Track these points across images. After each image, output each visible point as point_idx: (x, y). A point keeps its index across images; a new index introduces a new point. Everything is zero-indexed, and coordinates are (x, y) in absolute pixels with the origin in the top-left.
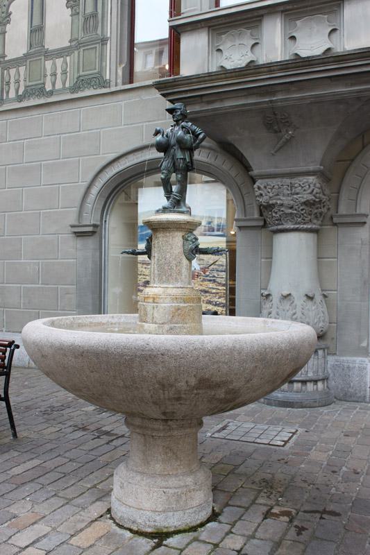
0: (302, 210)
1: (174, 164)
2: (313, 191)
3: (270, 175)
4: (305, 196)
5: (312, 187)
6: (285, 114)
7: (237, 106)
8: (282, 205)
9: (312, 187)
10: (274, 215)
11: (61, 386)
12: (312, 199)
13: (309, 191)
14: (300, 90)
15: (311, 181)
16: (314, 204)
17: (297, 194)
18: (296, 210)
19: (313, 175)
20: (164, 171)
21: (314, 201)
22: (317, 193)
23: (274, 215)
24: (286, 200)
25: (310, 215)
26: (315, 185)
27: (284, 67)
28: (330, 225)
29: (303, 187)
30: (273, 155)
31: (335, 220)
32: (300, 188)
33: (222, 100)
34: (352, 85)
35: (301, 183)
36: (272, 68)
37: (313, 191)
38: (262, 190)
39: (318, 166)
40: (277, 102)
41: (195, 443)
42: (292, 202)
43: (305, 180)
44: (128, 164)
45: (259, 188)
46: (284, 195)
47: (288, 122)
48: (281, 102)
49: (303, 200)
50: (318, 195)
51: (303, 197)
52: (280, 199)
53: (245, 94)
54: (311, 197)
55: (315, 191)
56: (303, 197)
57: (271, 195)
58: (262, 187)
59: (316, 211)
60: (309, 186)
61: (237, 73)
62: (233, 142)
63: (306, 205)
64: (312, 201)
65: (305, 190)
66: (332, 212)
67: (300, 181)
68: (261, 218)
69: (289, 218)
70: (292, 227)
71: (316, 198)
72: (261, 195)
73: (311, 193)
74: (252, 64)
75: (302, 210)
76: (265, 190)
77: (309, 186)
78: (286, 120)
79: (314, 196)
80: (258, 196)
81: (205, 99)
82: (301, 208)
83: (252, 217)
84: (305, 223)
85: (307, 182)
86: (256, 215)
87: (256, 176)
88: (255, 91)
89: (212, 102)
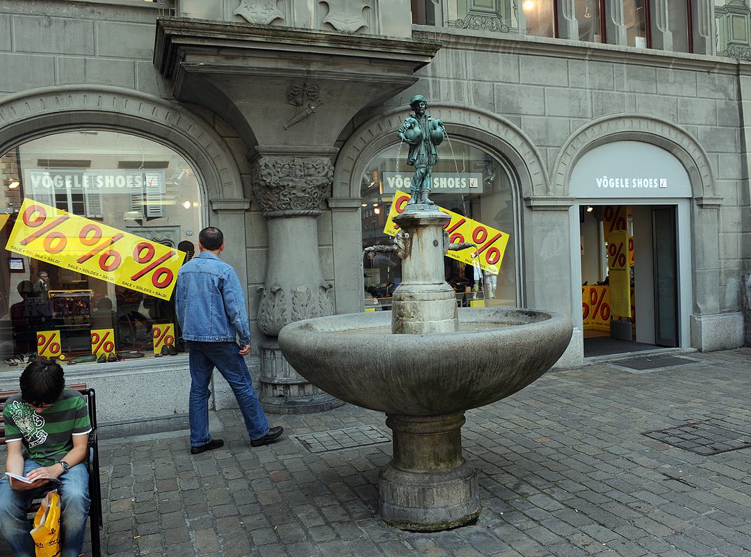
5: (326, 171)
6: (316, 87)
7: (267, 69)
8: (294, 187)
10: (282, 197)
11: (106, 439)
15: (325, 162)
17: (310, 176)
18: (308, 193)
19: (327, 156)
23: (282, 197)
24: (301, 183)
29: (316, 169)
30: (286, 129)
31: (332, 205)
33: (245, 58)
34: (389, 71)
35: (315, 164)
40: (314, 73)
41: (454, 438)
42: (305, 185)
44: (29, 114)
45: (266, 165)
46: (296, 176)
47: (313, 96)
48: (319, 74)
52: (292, 180)
53: (275, 56)
57: (281, 175)
58: (271, 166)
62: (239, 108)
69: (300, 202)
70: (302, 212)
73: (326, 175)
74: (276, 24)
78: (314, 94)
80: (265, 176)
81: (222, 53)
82: (315, 191)
84: (314, 208)
88: (288, 56)
89: (233, 58)
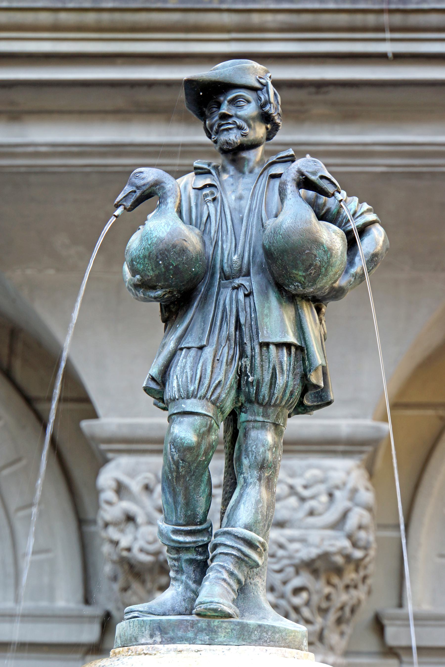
0: (297, 591)
1: (241, 374)
2: (345, 516)
3: (335, 442)
4: (314, 536)
5: (342, 501)
9: (342, 501)
12: (341, 552)
13: (332, 516)
14: (349, 115)
15: (337, 476)
16: (339, 571)
19: (345, 454)
20: (190, 405)
21: (348, 558)
22: (360, 527)
25: (323, 611)
26: (354, 491)
27: (306, 19)
28: (369, 654)
29: (303, 499)
32: (293, 501)
35: (298, 482)
36: (256, 18)
37: (345, 516)
38: (132, 498)
39: (369, 422)
43: (316, 472)
45: (120, 489)
49: (307, 553)
50: (362, 534)
51: (303, 540)
54: (339, 543)
55: (352, 522)
56: (303, 540)
58: (135, 486)
59: (344, 597)
60: (331, 495)
61: (106, 17)
63: (315, 572)
64: (339, 560)
65: (311, 513)
66: (383, 603)
67: (293, 475)
68: (88, 610)
71: (355, 545)
72: (130, 519)
73: (339, 524)
75: (297, 591)
76: (145, 498)
77: (331, 495)
79: (350, 537)
80: (116, 524)
82: (297, 582)
83: (44, 604)
85: (323, 481)
86: (66, 598)
87: (109, 441)
